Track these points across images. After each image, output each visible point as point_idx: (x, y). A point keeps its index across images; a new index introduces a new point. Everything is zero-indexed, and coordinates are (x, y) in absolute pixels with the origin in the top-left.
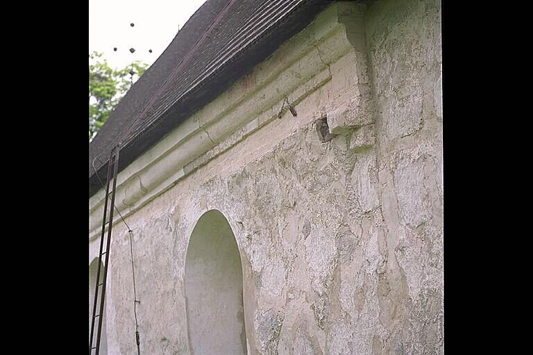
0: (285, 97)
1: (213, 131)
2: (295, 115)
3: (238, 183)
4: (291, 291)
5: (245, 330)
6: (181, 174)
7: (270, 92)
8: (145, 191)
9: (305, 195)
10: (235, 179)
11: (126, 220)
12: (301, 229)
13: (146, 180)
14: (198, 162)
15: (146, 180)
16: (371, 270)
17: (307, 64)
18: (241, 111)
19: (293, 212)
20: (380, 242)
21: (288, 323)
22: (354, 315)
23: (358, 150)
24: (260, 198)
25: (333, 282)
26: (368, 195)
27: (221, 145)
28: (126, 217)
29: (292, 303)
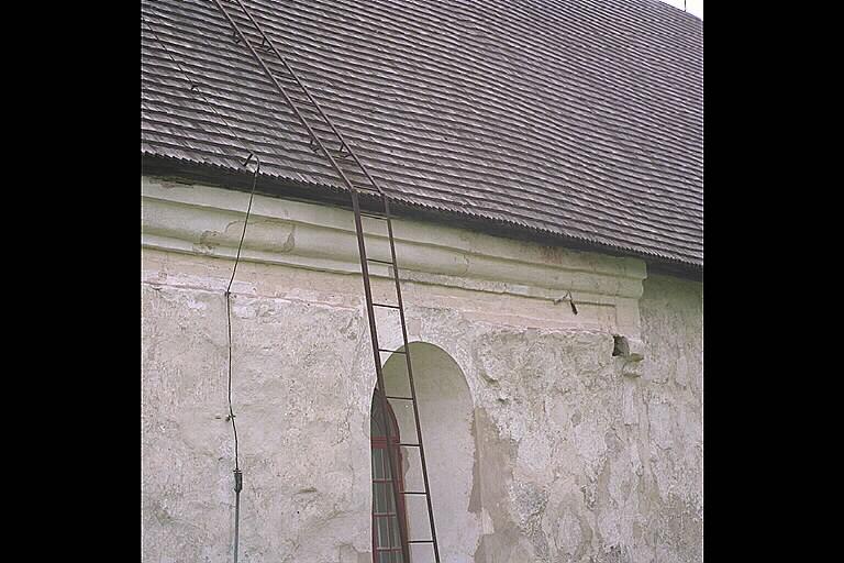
0: (569, 291)
1: (477, 264)
2: (575, 311)
3: (504, 339)
4: (558, 469)
5: (479, 484)
6: (189, 248)
7: (564, 279)
8: (288, 250)
9: (581, 387)
10: (504, 334)
11: (241, 268)
12: (570, 416)
13: (303, 239)
14: (421, 277)
15: (303, 239)
16: (634, 470)
17: (605, 283)
18: (524, 271)
19: (563, 398)
20: (323, 316)
21: (554, 500)
22: (621, 503)
23: (627, 375)
24: (529, 367)
25: (603, 475)
26: (630, 411)
27: (467, 280)
28: (244, 260)
29: (559, 482)
